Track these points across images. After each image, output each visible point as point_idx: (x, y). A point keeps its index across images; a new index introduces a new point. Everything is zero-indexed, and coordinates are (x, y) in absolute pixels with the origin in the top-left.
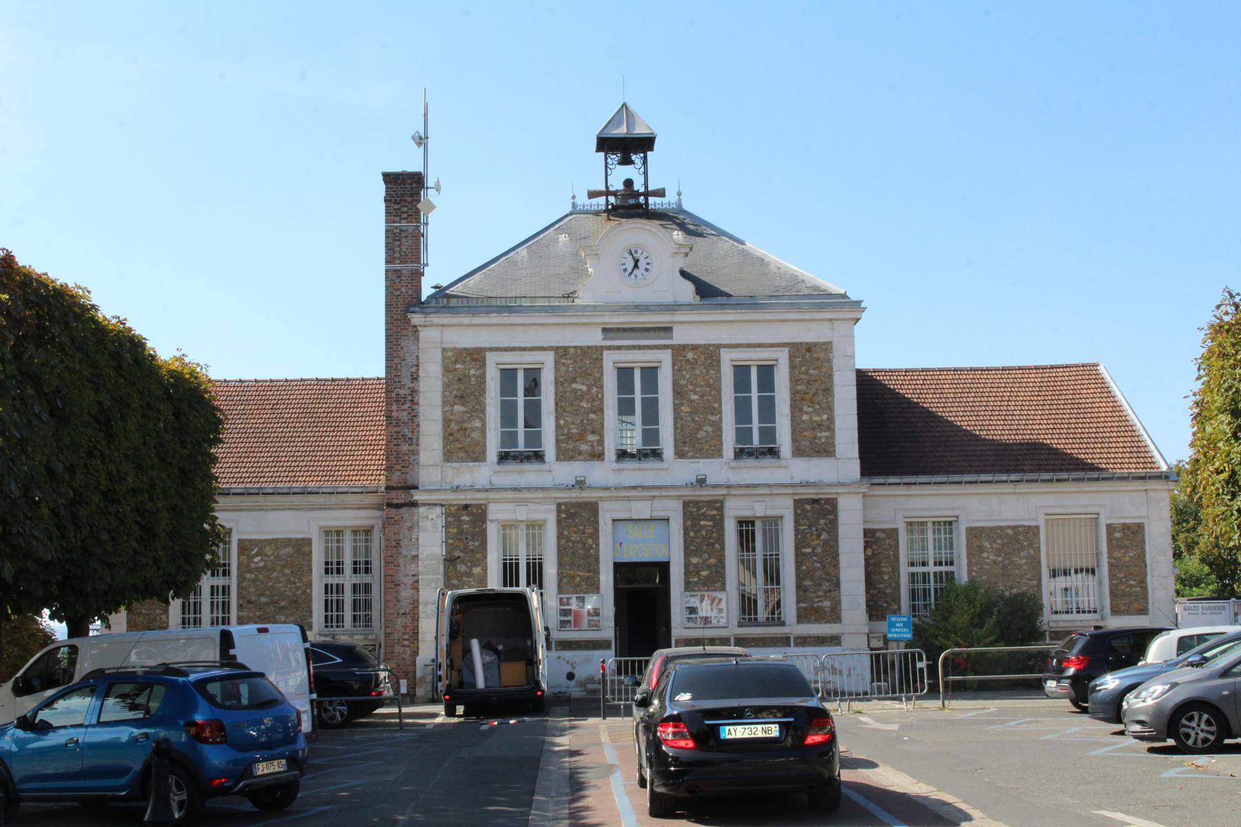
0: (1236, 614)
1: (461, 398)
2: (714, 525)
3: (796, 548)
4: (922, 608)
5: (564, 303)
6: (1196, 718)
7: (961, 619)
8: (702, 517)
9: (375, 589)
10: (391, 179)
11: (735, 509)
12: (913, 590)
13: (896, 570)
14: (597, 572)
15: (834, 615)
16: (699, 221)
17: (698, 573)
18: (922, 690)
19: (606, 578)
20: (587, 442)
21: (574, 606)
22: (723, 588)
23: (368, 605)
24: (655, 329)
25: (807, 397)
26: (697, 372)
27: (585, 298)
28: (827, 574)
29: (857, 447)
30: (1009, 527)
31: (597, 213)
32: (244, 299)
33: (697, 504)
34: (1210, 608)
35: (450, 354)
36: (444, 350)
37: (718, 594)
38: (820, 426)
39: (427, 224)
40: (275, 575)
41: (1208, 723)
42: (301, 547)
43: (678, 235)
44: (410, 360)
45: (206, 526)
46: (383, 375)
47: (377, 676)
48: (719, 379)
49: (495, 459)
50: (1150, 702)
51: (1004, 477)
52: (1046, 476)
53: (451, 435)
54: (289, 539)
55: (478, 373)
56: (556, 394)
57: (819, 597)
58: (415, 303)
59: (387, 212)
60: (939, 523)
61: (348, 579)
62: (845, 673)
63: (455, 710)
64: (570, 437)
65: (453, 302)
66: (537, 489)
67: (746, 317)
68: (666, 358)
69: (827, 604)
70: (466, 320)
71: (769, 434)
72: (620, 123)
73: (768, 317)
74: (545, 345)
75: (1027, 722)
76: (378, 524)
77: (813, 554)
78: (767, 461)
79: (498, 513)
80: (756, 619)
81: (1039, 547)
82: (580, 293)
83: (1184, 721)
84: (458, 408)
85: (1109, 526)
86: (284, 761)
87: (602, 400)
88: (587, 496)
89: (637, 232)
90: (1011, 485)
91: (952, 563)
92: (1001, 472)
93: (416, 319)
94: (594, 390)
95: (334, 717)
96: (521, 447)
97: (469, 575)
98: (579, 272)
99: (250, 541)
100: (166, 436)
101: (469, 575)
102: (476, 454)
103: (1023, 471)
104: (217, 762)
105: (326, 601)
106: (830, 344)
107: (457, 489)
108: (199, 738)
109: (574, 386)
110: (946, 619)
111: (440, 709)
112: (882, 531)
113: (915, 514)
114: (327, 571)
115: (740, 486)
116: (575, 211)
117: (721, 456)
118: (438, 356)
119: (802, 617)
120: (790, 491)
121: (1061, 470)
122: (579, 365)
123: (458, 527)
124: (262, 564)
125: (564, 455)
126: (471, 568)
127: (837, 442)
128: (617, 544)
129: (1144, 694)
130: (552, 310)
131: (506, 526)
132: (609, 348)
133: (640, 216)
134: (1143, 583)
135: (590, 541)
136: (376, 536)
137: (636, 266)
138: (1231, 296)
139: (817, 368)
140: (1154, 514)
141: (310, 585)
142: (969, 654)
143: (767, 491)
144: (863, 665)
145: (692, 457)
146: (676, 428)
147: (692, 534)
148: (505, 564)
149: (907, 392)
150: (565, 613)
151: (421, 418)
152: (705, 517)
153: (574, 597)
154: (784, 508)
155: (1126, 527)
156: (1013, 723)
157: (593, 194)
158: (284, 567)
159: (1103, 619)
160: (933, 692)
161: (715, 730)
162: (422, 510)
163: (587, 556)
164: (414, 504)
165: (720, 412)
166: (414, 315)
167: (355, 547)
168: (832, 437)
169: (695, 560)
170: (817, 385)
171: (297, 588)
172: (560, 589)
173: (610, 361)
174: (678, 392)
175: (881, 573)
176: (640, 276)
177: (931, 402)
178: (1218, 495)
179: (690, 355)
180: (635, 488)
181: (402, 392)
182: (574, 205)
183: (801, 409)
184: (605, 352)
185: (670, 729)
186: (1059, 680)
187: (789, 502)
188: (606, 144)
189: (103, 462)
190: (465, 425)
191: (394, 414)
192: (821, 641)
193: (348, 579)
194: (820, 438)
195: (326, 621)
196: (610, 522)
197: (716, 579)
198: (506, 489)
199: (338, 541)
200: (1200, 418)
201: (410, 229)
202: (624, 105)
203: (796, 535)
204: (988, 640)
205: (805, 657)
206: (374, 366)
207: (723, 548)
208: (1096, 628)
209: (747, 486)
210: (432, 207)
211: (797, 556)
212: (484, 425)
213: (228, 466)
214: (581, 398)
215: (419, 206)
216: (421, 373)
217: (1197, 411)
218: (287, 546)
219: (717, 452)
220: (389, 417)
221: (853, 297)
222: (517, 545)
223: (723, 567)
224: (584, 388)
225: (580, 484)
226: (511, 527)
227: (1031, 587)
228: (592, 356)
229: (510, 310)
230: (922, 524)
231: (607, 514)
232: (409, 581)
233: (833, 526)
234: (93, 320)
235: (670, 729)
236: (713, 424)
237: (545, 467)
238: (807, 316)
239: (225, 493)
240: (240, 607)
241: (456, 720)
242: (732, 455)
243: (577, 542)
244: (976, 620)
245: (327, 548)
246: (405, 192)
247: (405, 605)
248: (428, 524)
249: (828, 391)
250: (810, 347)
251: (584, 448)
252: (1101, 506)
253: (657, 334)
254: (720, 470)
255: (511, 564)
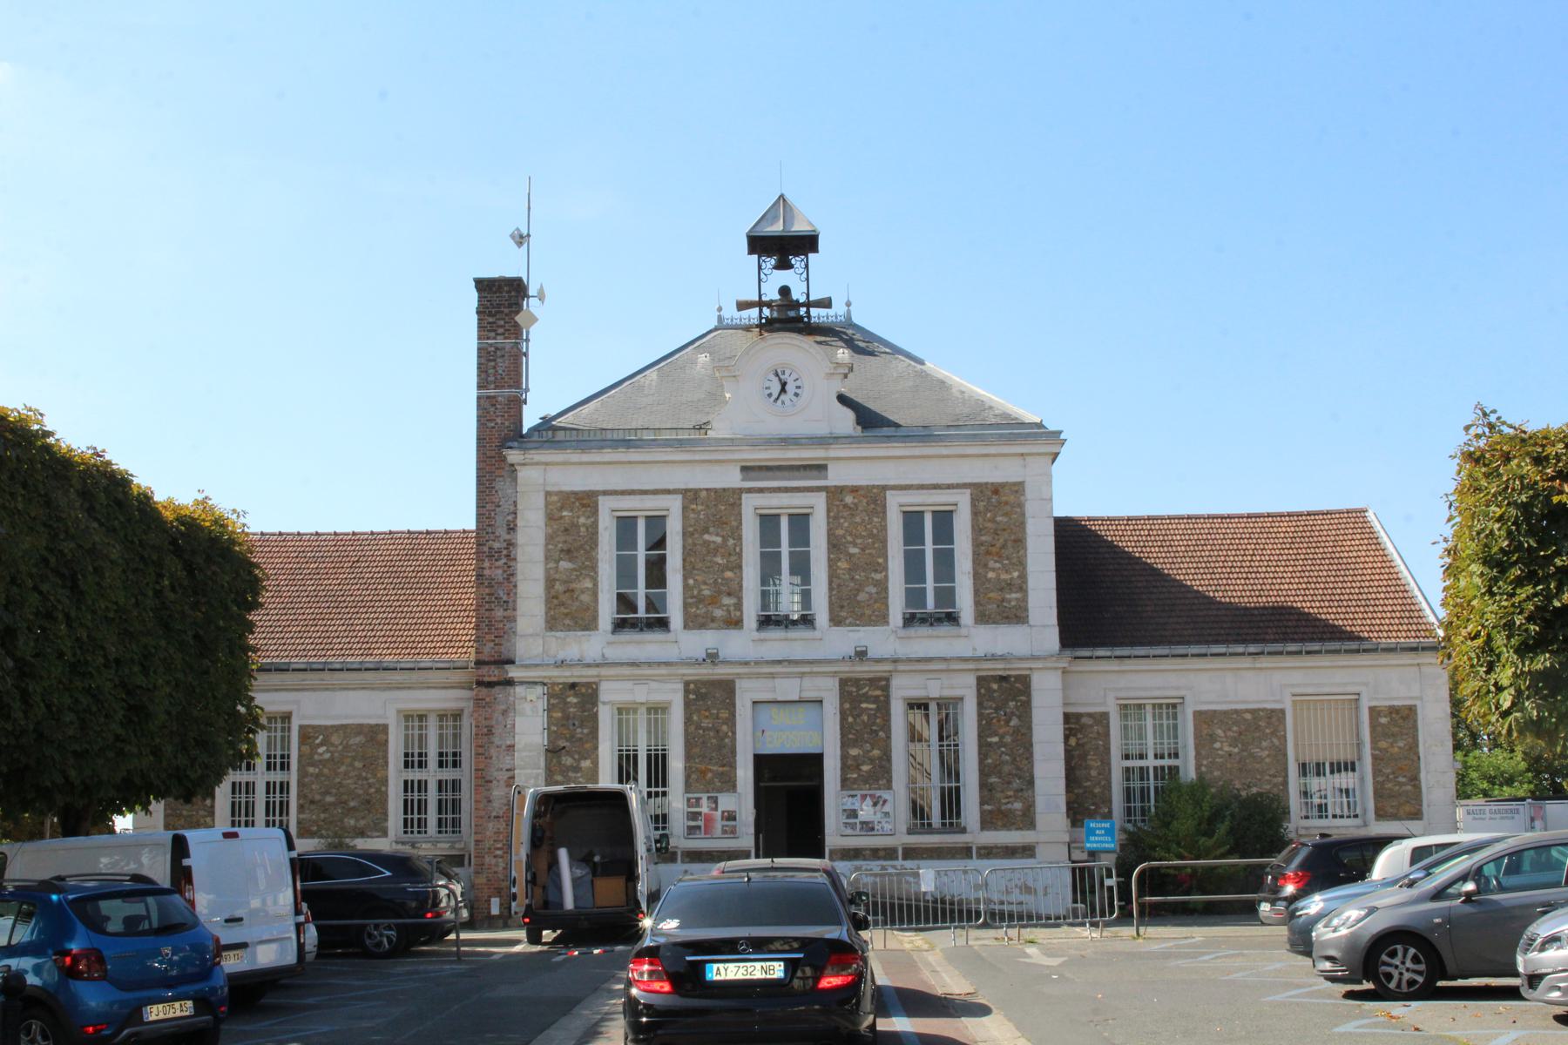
0: (1532, 820)
1: (568, 553)
2: (878, 709)
3: (980, 736)
4: (1139, 812)
5: (695, 435)
6: (1400, 954)
7: (1184, 825)
8: (864, 700)
9: (465, 786)
10: (485, 286)
11: (904, 688)
12: (1128, 789)
13: (1106, 763)
14: (733, 766)
15: (1027, 820)
16: (871, 337)
17: (858, 767)
18: (1111, 913)
19: (745, 774)
20: (721, 606)
21: (705, 808)
22: (889, 786)
23: (456, 805)
24: (805, 467)
25: (994, 550)
26: (858, 519)
27: (718, 431)
28: (1018, 768)
29: (1055, 611)
30: (1247, 711)
31: (748, 328)
32: (294, 430)
33: (857, 682)
34: (1499, 812)
35: (555, 498)
36: (548, 494)
37: (885, 795)
38: (1010, 586)
39: (527, 340)
40: (343, 769)
41: (1415, 960)
42: (375, 735)
43: (843, 354)
44: (506, 507)
45: (242, 710)
46: (473, 527)
47: (436, 894)
48: (884, 528)
49: (609, 627)
50: (1344, 931)
51: (1240, 649)
52: (1292, 647)
53: (556, 597)
54: (361, 726)
55: (589, 522)
56: (684, 547)
57: (1008, 796)
58: (515, 436)
59: (481, 327)
60: (1160, 705)
61: (432, 774)
62: (1041, 893)
63: (541, 936)
64: (700, 600)
65: (560, 435)
66: (659, 664)
67: (917, 452)
68: (819, 503)
69: (1018, 805)
70: (575, 457)
71: (946, 596)
72: (776, 219)
73: (945, 451)
74: (671, 487)
75: (1232, 956)
76: (468, 707)
77: (1001, 744)
78: (945, 629)
79: (612, 693)
80: (930, 825)
81: (1285, 737)
82: (714, 424)
83: (1384, 958)
84: (564, 565)
85: (1372, 709)
86: (190, 1003)
87: (740, 555)
88: (721, 672)
89: (790, 349)
90: (1249, 659)
91: (1176, 756)
92: (1237, 642)
93: (513, 456)
94: (731, 542)
95: (380, 944)
96: (642, 613)
97: (577, 769)
98: (716, 398)
99: (313, 727)
100: (172, 596)
101: (577, 769)
102: (585, 621)
103: (1263, 641)
104: (93, 1004)
105: (406, 801)
106: (1021, 484)
107: (562, 664)
108: (71, 973)
109: (706, 537)
110: (1167, 825)
111: (521, 934)
112: (1090, 715)
113: (1132, 694)
114: (406, 765)
115: (909, 660)
116: (722, 326)
117: (887, 623)
118: (540, 501)
119: (987, 822)
120: (971, 666)
121: (1312, 640)
122: (713, 511)
123: (563, 711)
124: (327, 756)
125: (692, 622)
126: (578, 761)
127: (1030, 605)
128: (758, 731)
129: (1335, 922)
130: (680, 444)
131: (622, 710)
132: (750, 490)
133: (799, 331)
134: (1415, 779)
135: (725, 728)
136: (466, 722)
137: (783, 390)
138: (1485, 415)
139: (1006, 514)
140: (1426, 691)
141: (385, 781)
142: (1193, 868)
143: (943, 666)
144: (1064, 881)
145: (851, 625)
146: (831, 589)
147: (850, 719)
148: (620, 757)
149: (1128, 545)
150: (694, 816)
151: (519, 577)
152: (867, 698)
153: (704, 797)
154: (964, 688)
155: (1393, 711)
156: (1206, 958)
157: (743, 306)
158: (354, 758)
159: (1365, 825)
160: (1125, 918)
161: (699, 968)
162: (519, 690)
163: (720, 747)
164: (510, 683)
165: (885, 569)
166: (510, 452)
167: (441, 736)
168: (1025, 599)
169: (854, 752)
170: (1006, 535)
171: (370, 786)
172: (688, 787)
173: (750, 506)
174: (834, 545)
175: (1088, 768)
176: (787, 402)
177: (1156, 557)
178: (1472, 666)
179: (849, 499)
180: (779, 662)
181: (496, 545)
182: (720, 319)
183: (986, 565)
184: (744, 496)
185: (646, 967)
186: (1273, 902)
187: (971, 680)
188: (760, 244)
189: (69, 626)
190: (573, 586)
191: (487, 572)
192: (1010, 852)
193: (432, 774)
194: (1009, 601)
195: (406, 826)
196: (749, 704)
197: (881, 774)
198: (622, 664)
199: (421, 728)
200: (1451, 571)
201: (508, 347)
202: (782, 196)
203: (979, 721)
204: (1218, 852)
205: (965, 872)
206: (460, 514)
207: (889, 737)
208: (1323, 836)
209: (919, 660)
210: (534, 320)
211: (980, 746)
212: (596, 585)
213: (271, 632)
214: (715, 551)
215: (517, 318)
216: (520, 523)
217: (1448, 560)
218: (359, 734)
219: (883, 619)
220: (479, 576)
221: (1051, 427)
222: (635, 732)
223: (889, 760)
224: (719, 540)
225: (712, 658)
226: (628, 711)
227: (1275, 785)
228: (728, 500)
229: (627, 444)
230: (1140, 706)
231: (746, 694)
232: (504, 776)
233: (1025, 709)
234: (48, 448)
235: (646, 967)
236: (877, 583)
237: (670, 636)
238: (992, 450)
239: (264, 669)
240: (301, 808)
241: (539, 948)
242: (900, 622)
243: (708, 729)
244: (1204, 826)
245: (407, 736)
246: (502, 302)
247: (497, 807)
248: (527, 707)
249: (1020, 542)
250: (996, 489)
251: (718, 613)
252: (1366, 684)
253: (808, 473)
254: (884, 641)
255: (628, 756)
